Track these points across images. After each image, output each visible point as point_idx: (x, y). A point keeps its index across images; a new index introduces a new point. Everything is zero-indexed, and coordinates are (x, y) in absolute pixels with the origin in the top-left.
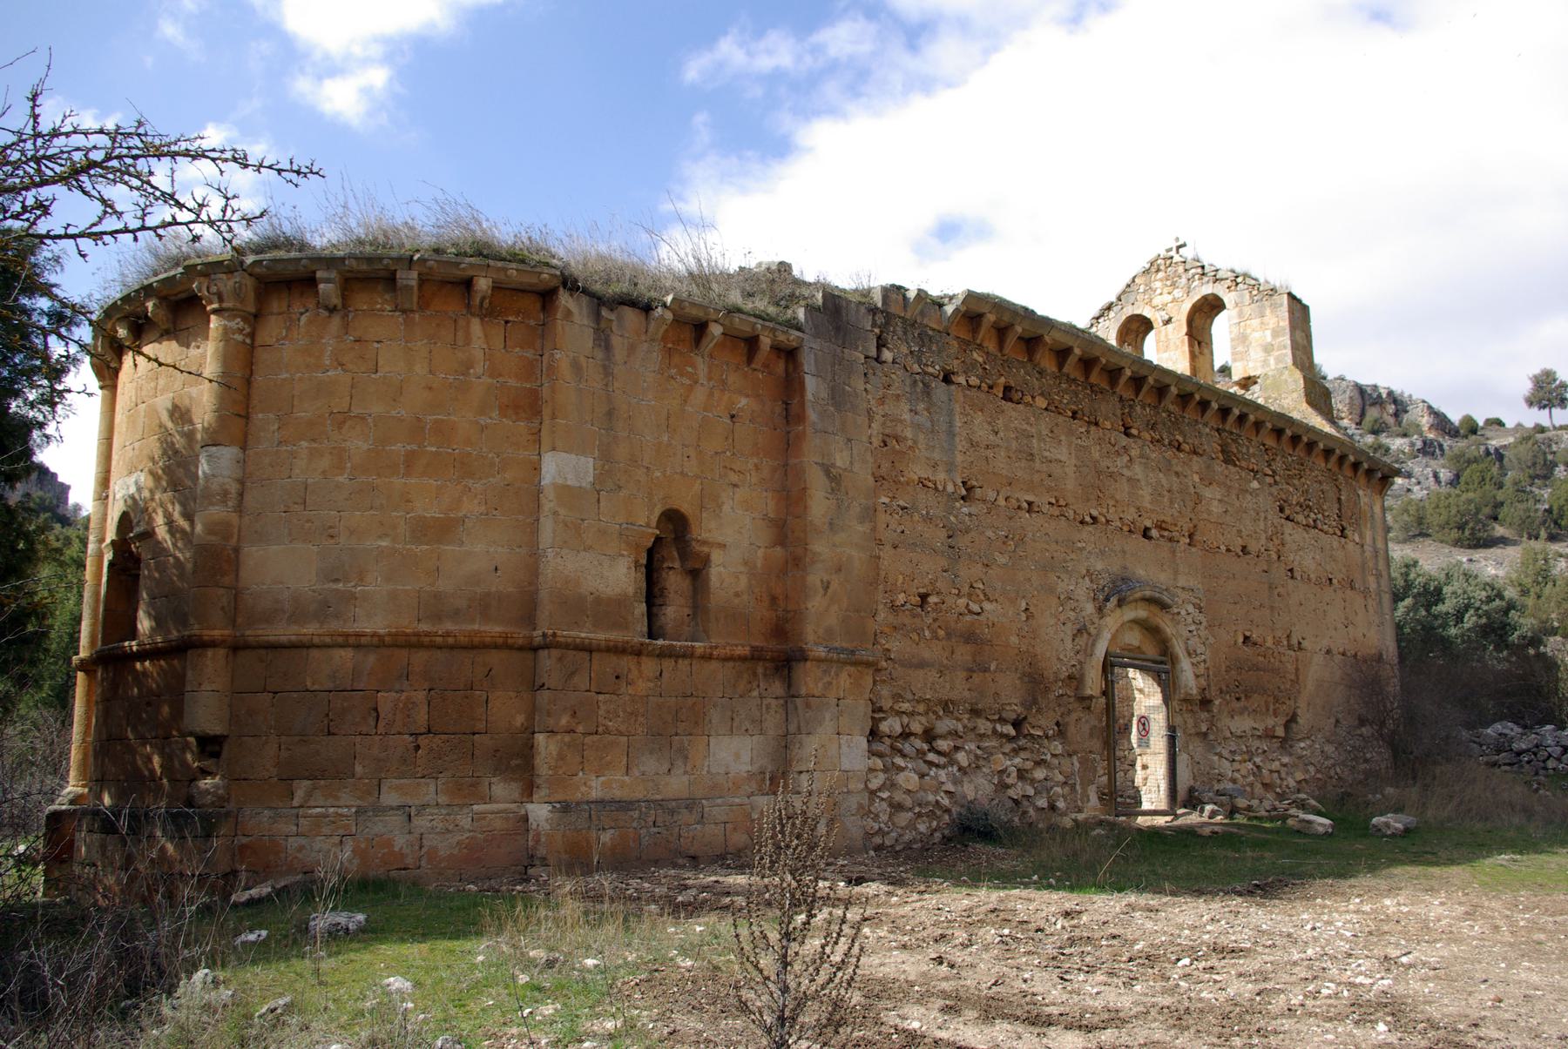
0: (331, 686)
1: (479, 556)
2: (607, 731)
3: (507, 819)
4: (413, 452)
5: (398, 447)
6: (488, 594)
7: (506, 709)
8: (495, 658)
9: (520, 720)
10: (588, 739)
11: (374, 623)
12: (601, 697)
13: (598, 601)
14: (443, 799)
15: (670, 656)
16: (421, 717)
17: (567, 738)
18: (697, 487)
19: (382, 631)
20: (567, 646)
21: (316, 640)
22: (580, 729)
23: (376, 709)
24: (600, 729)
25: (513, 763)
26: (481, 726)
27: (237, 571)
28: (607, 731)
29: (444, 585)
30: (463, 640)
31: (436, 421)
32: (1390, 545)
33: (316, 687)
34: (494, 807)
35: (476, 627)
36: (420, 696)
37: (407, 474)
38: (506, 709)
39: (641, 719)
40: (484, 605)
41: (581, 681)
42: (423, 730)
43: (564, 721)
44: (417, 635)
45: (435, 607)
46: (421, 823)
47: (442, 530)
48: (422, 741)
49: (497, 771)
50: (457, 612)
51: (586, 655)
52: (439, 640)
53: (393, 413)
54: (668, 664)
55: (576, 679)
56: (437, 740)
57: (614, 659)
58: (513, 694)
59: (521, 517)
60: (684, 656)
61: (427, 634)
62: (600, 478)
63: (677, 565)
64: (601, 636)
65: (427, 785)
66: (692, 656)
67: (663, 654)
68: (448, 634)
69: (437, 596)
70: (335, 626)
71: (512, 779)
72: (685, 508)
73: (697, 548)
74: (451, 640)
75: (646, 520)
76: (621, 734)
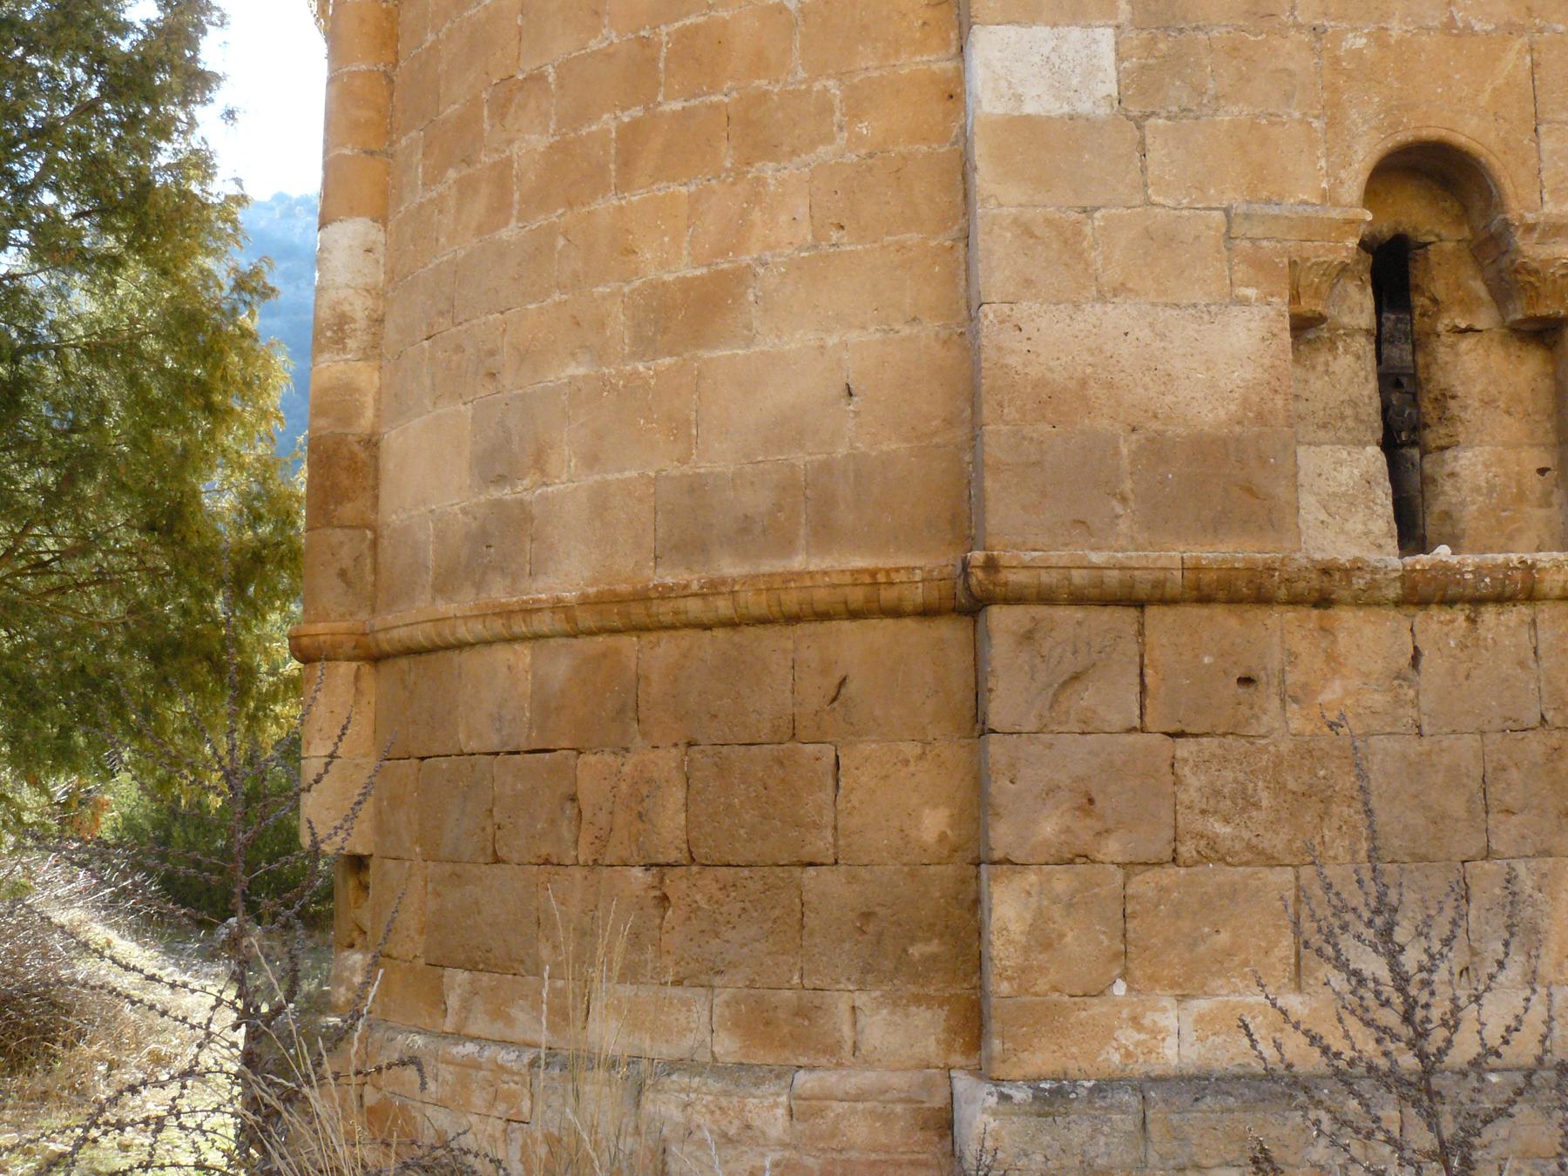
0: (494, 742)
1: (816, 358)
2: (1214, 853)
3: (887, 1118)
4: (635, 124)
5: (608, 122)
6: (826, 467)
7: (896, 802)
8: (854, 643)
9: (933, 824)
10: (1144, 884)
11: (568, 576)
12: (1184, 748)
13: (1156, 449)
14: (727, 1046)
15: (1449, 602)
16: (671, 822)
17: (1063, 881)
18: (1513, 60)
19: (570, 596)
20: (1046, 598)
21: (463, 632)
22: (1113, 848)
23: (573, 799)
24: (1187, 850)
25: (916, 951)
26: (821, 844)
27: (376, 487)
28: (1214, 853)
29: (718, 458)
30: (754, 602)
31: (684, 34)
32: (358, 979)
33: (473, 745)
34: (856, 1080)
35: (797, 563)
36: (666, 761)
37: (625, 185)
38: (896, 802)
39: (1341, 810)
40: (814, 505)
41: (1112, 699)
42: (673, 856)
43: (1049, 828)
44: (642, 597)
45: (689, 520)
46: (664, 1107)
47: (700, 310)
48: (676, 884)
49: (867, 974)
50: (745, 526)
51: (1125, 618)
52: (694, 607)
53: (594, 45)
54: (1441, 628)
55: (1087, 697)
56: (708, 881)
57: (1223, 621)
58: (910, 749)
59: (912, 238)
60: (1501, 599)
61: (666, 593)
62: (1143, 87)
63: (1485, 318)
64: (1171, 556)
65: (686, 1004)
66: (1531, 596)
67: (1417, 596)
68: (714, 588)
69: (696, 487)
70: (499, 592)
71: (917, 1000)
72: (1468, 130)
73: (1531, 250)
74: (723, 607)
75: (1327, 190)
76: (1271, 861)
